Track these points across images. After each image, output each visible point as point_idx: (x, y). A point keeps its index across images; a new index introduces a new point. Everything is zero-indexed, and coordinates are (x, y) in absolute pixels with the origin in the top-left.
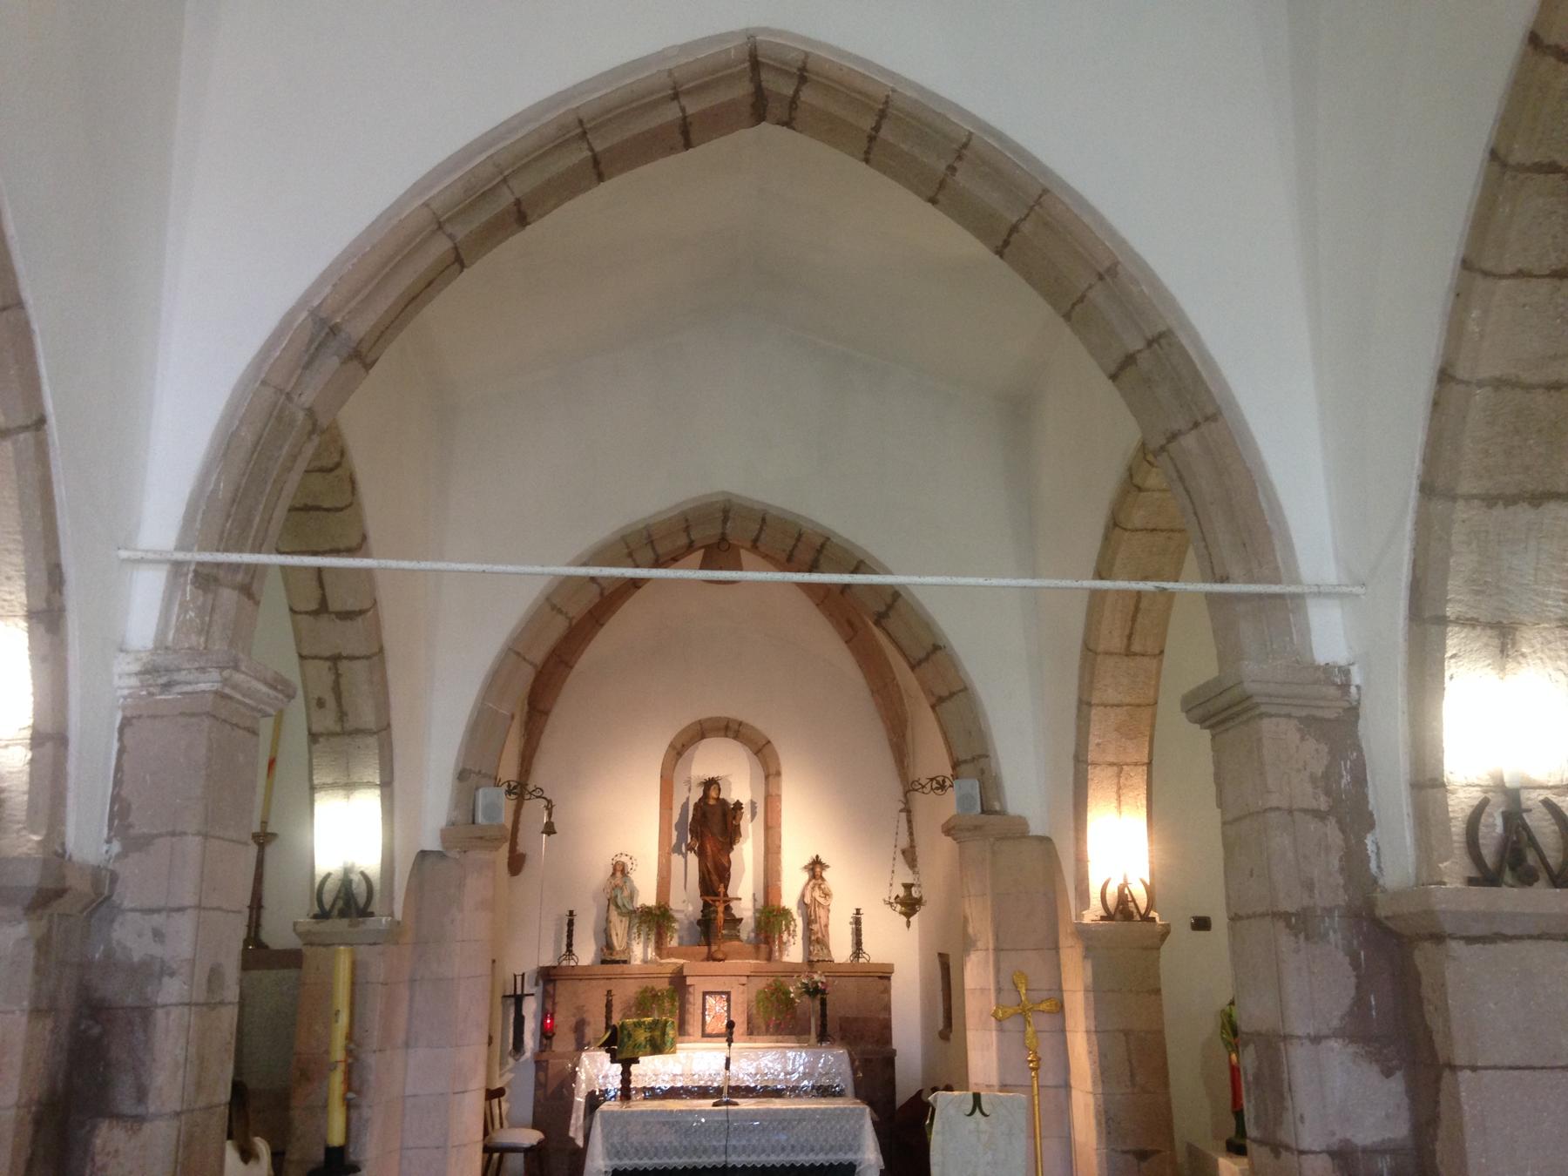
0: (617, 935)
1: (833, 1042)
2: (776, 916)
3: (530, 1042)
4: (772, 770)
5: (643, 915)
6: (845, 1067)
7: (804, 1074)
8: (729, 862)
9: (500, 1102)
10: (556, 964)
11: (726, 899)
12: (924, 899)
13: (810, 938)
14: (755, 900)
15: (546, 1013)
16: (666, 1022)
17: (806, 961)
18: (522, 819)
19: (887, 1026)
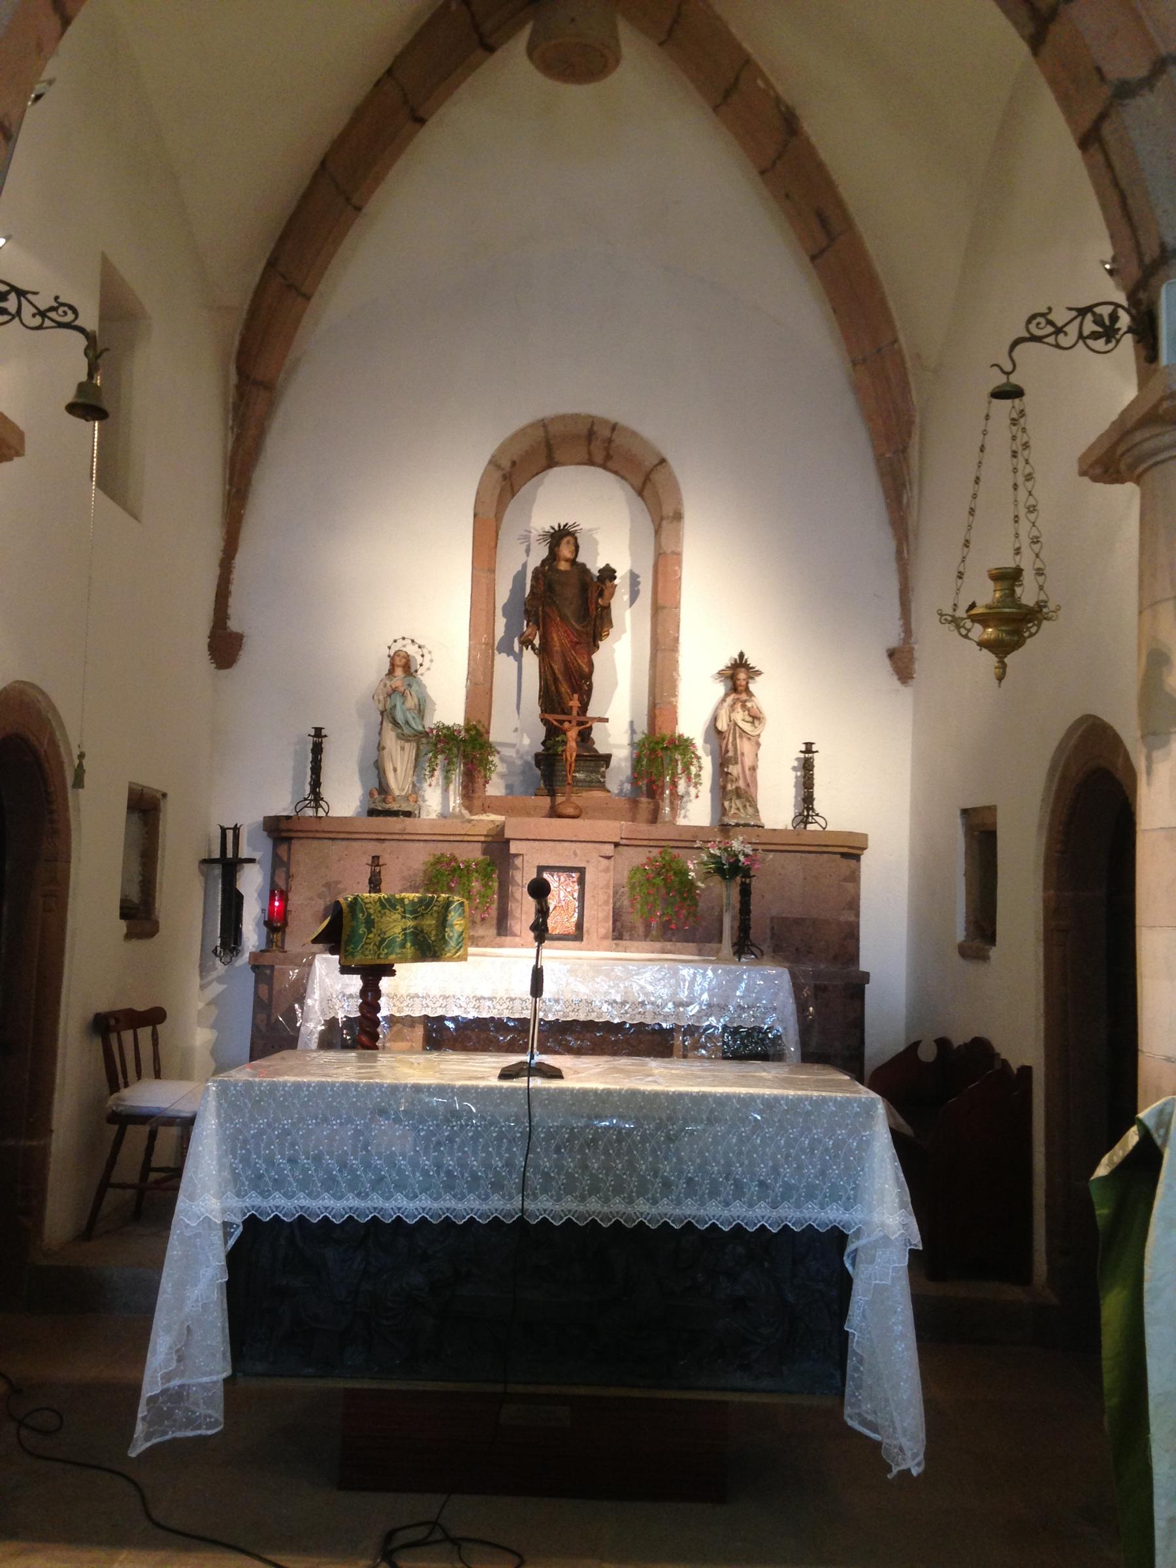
0: (395, 770)
1: (760, 956)
2: (666, 748)
3: (252, 935)
4: (668, 510)
5: (440, 741)
6: (786, 1000)
7: (709, 1005)
8: (591, 665)
9: (155, 1036)
10: (293, 814)
11: (582, 719)
12: (1052, 606)
13: (724, 788)
14: (633, 731)
15: (278, 892)
16: (448, 903)
17: (717, 824)
18: (236, 576)
19: (851, 934)
